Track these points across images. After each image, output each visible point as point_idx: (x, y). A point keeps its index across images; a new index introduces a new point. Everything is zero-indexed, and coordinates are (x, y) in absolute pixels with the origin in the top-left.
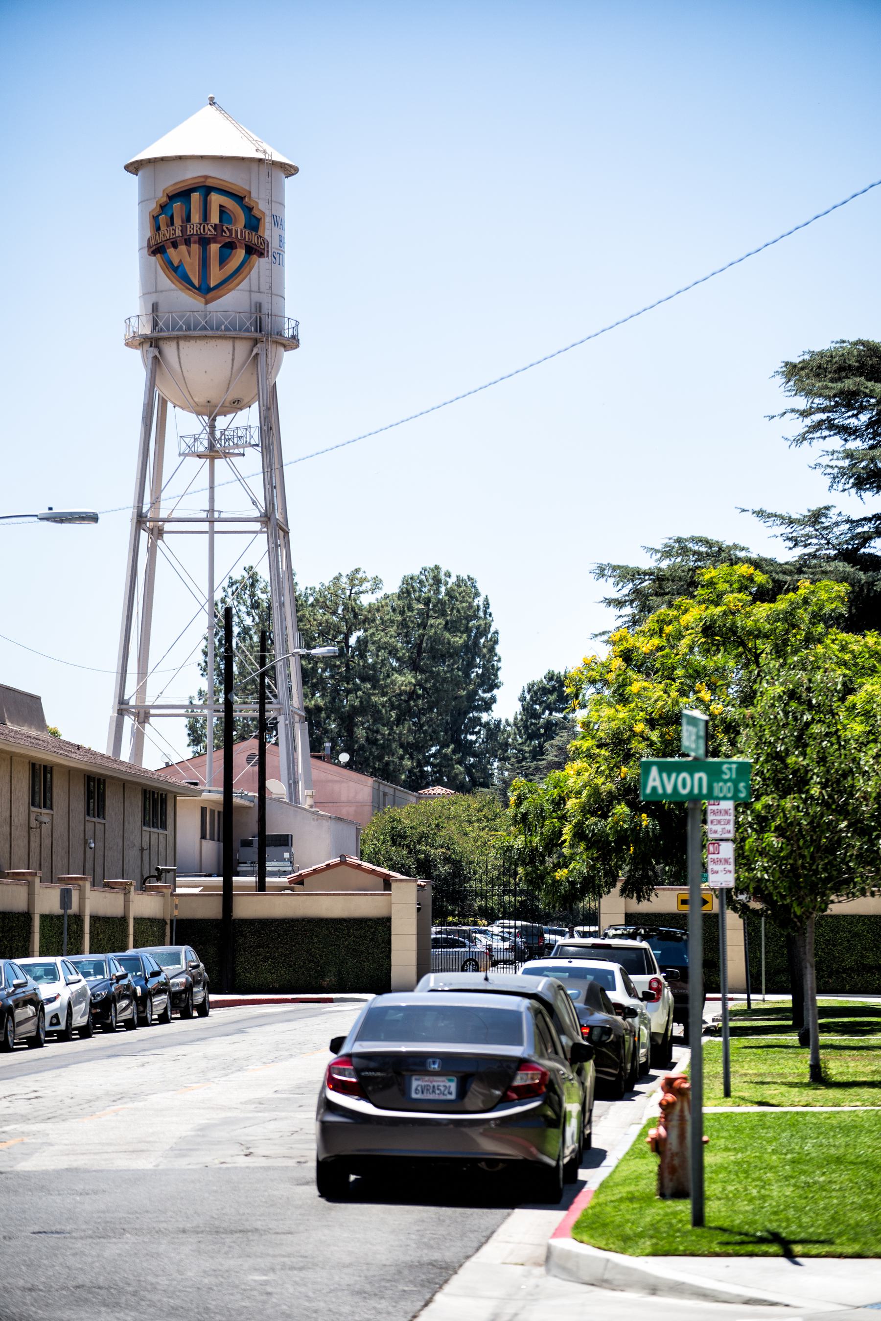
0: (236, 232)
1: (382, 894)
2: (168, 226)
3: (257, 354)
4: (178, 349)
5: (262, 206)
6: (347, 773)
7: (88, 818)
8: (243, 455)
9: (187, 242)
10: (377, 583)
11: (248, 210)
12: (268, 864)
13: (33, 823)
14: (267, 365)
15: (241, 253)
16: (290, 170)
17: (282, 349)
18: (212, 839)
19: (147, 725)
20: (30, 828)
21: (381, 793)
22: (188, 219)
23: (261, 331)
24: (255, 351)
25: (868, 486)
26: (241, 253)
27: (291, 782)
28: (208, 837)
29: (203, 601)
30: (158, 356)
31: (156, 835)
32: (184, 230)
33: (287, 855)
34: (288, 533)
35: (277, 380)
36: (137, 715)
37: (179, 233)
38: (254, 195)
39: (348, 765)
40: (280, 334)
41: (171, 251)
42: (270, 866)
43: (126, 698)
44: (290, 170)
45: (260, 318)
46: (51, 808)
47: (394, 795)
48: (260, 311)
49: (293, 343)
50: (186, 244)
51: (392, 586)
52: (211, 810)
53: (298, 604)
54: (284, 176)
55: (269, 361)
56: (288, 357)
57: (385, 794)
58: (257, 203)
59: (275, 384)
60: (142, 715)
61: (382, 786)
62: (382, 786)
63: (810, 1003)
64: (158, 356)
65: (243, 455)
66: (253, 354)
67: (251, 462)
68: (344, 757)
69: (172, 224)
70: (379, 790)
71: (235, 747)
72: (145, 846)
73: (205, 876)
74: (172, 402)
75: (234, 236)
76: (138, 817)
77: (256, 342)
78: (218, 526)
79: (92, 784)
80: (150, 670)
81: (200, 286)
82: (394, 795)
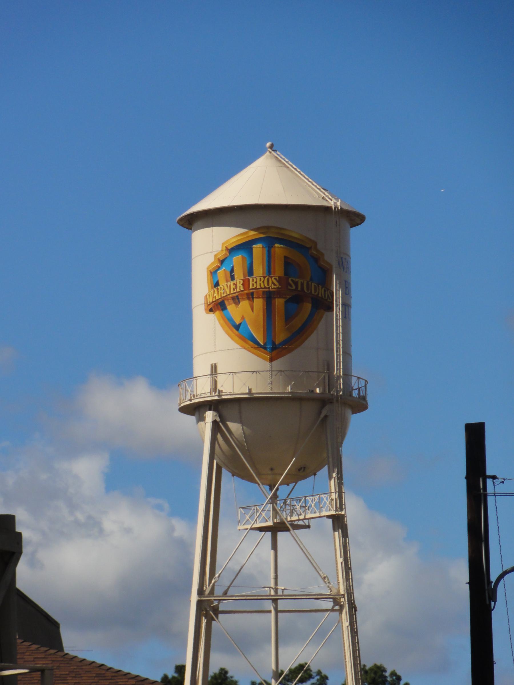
0: (302, 284)
1: (346, 316)
2: (227, 281)
3: (326, 417)
5: (330, 258)
8: (309, 527)
9: (251, 297)
11: (316, 259)
15: (308, 307)
16: (355, 219)
17: (349, 411)
22: (250, 272)
24: (324, 413)
25: (493, 603)
26: (308, 307)
30: (218, 419)
32: (246, 283)
37: (240, 287)
38: (320, 246)
41: (231, 308)
44: (355, 219)
49: (360, 405)
50: (248, 299)
54: (348, 225)
58: (323, 254)
63: (44, 665)
64: (218, 419)
66: (322, 416)
69: (233, 278)
75: (299, 289)
81: (265, 344)
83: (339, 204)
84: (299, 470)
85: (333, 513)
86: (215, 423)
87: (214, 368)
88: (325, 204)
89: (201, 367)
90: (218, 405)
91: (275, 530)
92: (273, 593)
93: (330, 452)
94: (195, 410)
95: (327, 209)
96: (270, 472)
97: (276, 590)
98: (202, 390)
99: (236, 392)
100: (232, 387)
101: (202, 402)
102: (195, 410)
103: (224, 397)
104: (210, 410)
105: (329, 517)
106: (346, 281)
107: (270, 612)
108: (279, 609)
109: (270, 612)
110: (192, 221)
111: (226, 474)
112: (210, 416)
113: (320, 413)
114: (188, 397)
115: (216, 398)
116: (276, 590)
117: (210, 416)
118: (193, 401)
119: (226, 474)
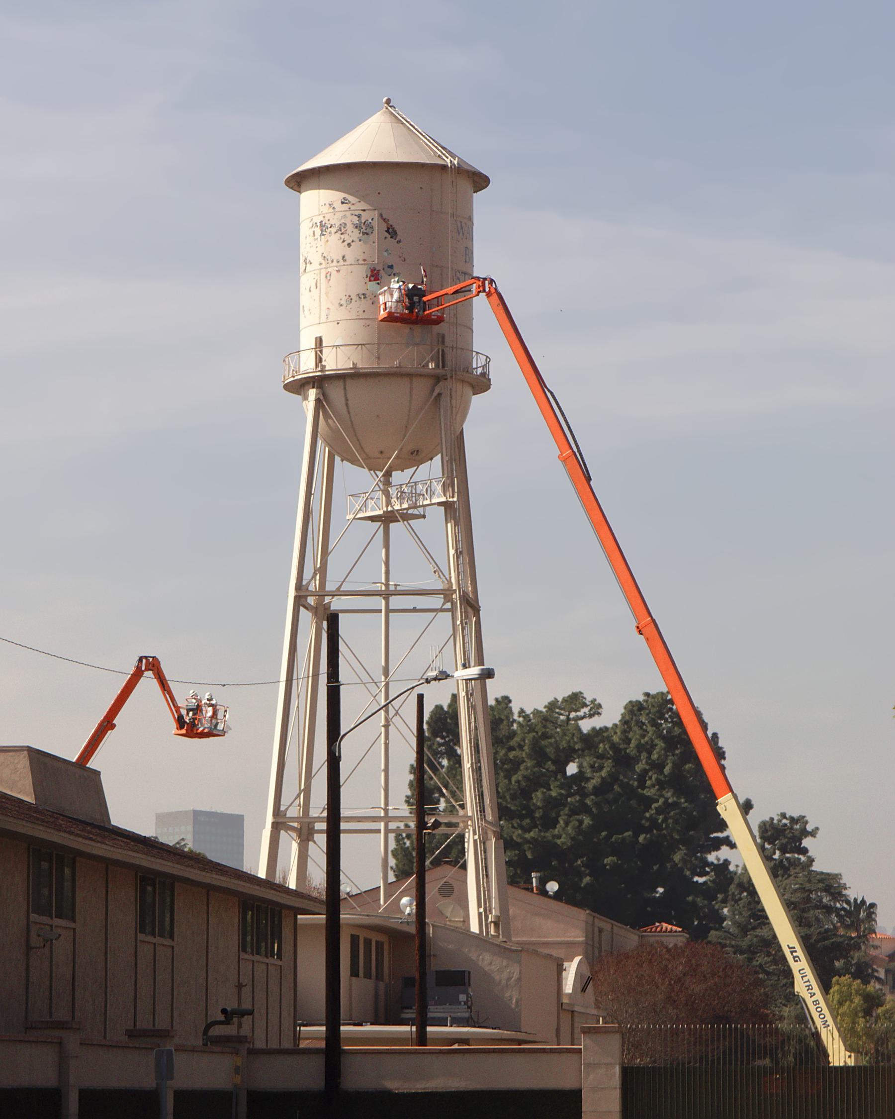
3: (439, 394)
4: (345, 389)
6: (554, 904)
7: (141, 937)
8: (424, 516)
10: (596, 710)
12: (431, 1008)
13: (35, 941)
14: (452, 407)
16: (480, 181)
17: (468, 390)
18: (368, 975)
19: (310, 843)
20: (29, 948)
21: (596, 929)
23: (443, 367)
27: (482, 910)
28: (361, 973)
29: (396, 720)
30: (322, 398)
31: (264, 967)
33: (462, 997)
34: (479, 611)
35: (464, 427)
36: (299, 832)
39: (557, 896)
40: (468, 369)
42: (434, 1012)
43: (282, 808)
44: (480, 181)
45: (443, 351)
46: (74, 920)
47: (612, 932)
48: (443, 343)
51: (611, 716)
52: (377, 942)
53: (498, 717)
55: (454, 402)
56: (477, 401)
57: (601, 931)
59: (462, 432)
60: (305, 831)
61: (596, 920)
62: (596, 920)
64: (322, 398)
65: (424, 516)
66: (435, 394)
67: (438, 531)
68: (553, 887)
70: (593, 924)
71: (428, 876)
72: (244, 980)
73: (355, 1025)
74: (340, 455)
76: (234, 939)
77: (438, 379)
78: (396, 602)
79: (150, 889)
80: (313, 773)
82: (612, 932)
83: (456, 162)
84: (412, 453)
85: (443, 499)
86: (318, 401)
87: (319, 341)
88: (441, 162)
89: (307, 341)
90: (320, 381)
91: (387, 519)
92: (383, 588)
93: (443, 432)
94: (298, 387)
95: (444, 167)
96: (380, 456)
97: (387, 585)
98: (307, 365)
99: (339, 367)
100: (334, 362)
101: (305, 378)
102: (298, 387)
103: (327, 373)
104: (313, 387)
105: (440, 504)
106: (467, 248)
107: (380, 611)
108: (450, 613)
109: (380, 611)
110: (299, 181)
111: (337, 459)
112: (312, 393)
113: (433, 390)
114: (291, 375)
115: (319, 374)
116: (387, 585)
117: (312, 393)
118: (296, 378)
119: (337, 459)
